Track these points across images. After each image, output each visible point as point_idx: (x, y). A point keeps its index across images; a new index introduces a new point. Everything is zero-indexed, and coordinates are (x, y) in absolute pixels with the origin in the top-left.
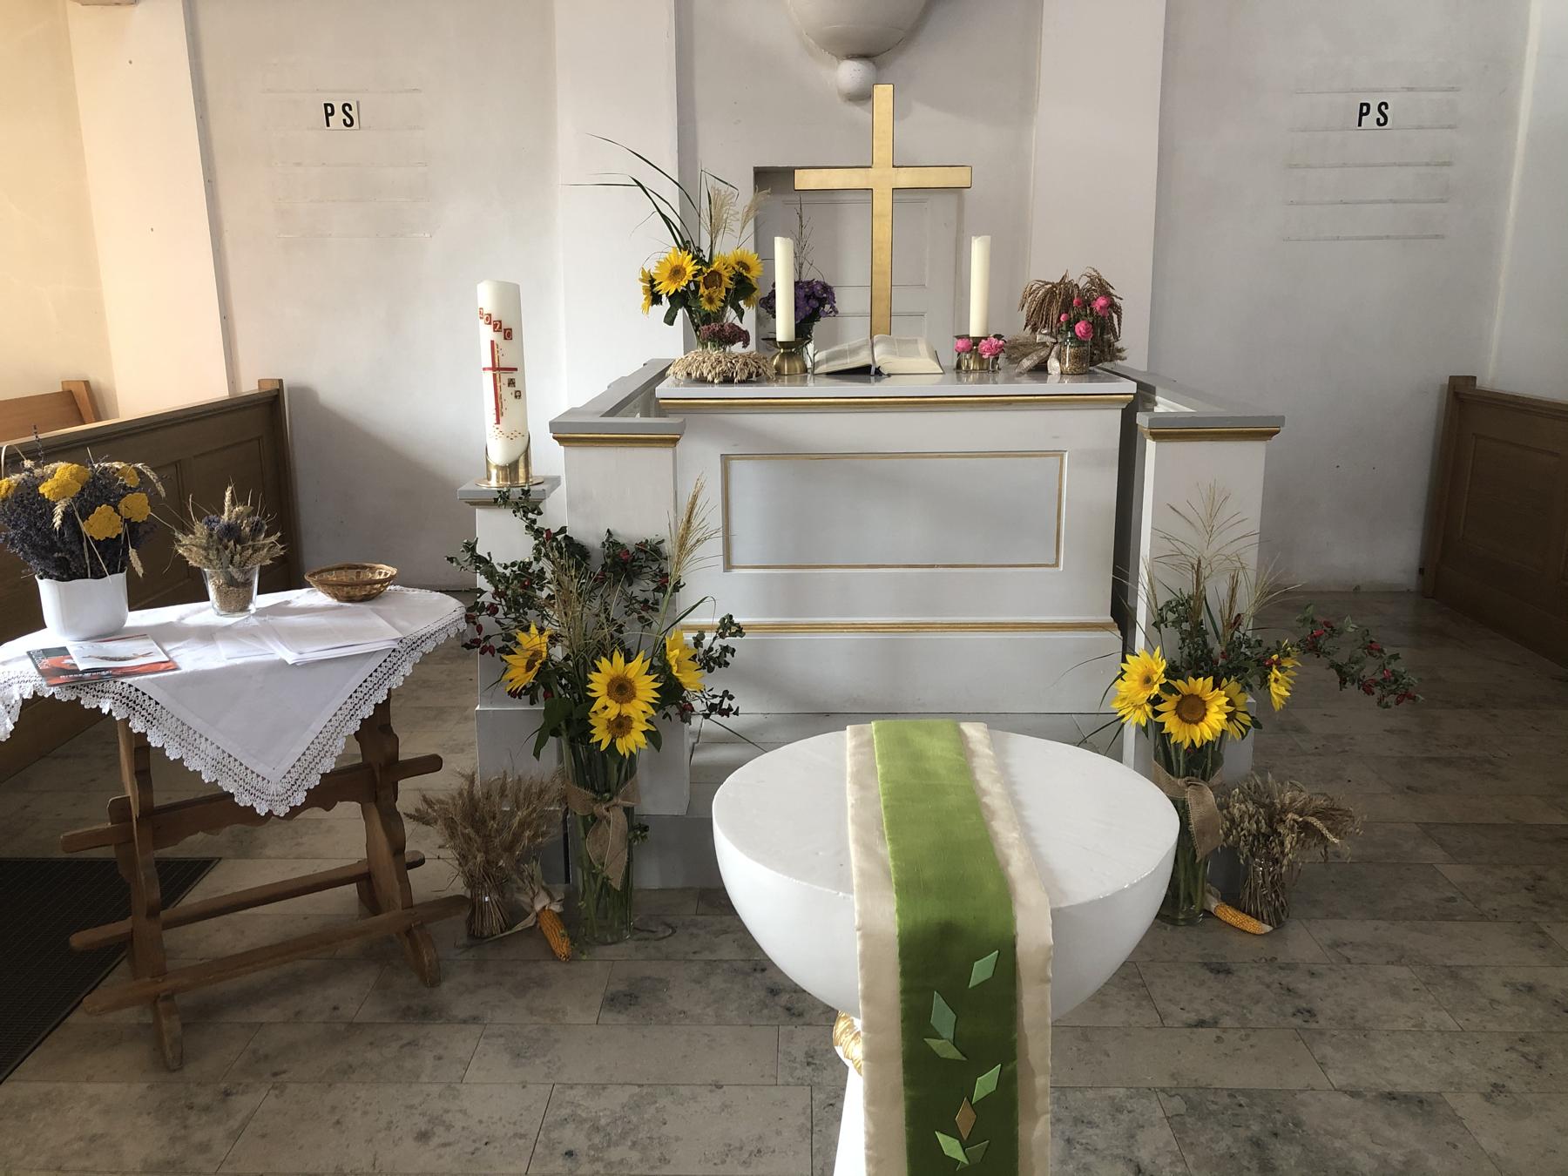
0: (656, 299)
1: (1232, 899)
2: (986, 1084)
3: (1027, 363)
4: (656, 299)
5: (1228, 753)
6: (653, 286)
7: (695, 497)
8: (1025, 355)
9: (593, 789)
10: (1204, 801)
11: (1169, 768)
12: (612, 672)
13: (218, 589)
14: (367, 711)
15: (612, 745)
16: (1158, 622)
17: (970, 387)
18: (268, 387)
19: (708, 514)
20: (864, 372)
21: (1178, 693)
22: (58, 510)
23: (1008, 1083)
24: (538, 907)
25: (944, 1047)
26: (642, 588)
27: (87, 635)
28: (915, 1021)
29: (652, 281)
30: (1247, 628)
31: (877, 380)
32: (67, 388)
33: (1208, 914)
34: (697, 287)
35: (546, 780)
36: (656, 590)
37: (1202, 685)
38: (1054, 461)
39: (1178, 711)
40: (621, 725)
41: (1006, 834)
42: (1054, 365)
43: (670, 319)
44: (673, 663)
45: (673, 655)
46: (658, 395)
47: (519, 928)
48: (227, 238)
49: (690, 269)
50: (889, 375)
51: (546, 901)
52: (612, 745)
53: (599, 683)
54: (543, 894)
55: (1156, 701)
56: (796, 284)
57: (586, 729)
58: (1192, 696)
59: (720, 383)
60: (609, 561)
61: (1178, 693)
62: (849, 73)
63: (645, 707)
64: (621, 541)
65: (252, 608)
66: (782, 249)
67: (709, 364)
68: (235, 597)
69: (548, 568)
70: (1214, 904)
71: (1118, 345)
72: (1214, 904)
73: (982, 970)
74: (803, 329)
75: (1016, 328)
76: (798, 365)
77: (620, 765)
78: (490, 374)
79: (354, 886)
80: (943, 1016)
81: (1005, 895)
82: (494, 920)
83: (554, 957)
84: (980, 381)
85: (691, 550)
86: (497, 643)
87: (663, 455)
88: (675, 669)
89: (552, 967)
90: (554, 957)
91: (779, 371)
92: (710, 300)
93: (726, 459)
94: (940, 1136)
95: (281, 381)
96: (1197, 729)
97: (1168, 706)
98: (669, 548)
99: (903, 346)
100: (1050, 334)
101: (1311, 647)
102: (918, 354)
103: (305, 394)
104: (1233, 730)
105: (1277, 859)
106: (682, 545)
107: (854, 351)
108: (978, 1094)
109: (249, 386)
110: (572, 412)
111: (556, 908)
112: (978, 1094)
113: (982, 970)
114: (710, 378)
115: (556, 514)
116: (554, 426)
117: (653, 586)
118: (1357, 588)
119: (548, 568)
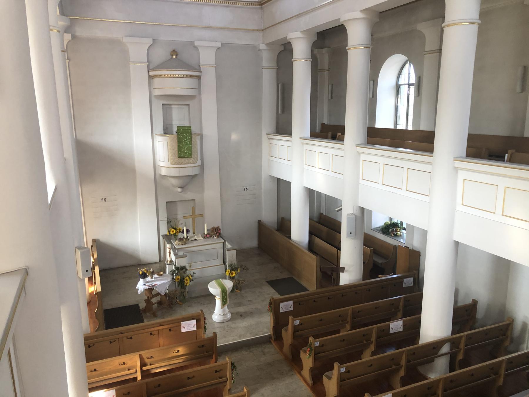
1: (237, 289)
5: (235, 277)
10: (234, 281)
11: (231, 279)
16: (229, 266)
25: (224, 295)
26: (184, 270)
30: (236, 266)
37: (233, 272)
39: (231, 274)
40: (187, 283)
41: (225, 285)
42: (215, 237)
55: (230, 273)
70: (236, 290)
72: (236, 290)
73: (225, 291)
80: (224, 294)
81: (226, 288)
83: (181, 305)
90: (181, 305)
97: (230, 274)
101: (241, 267)
104: (236, 275)
105: (142, 273)
113: (225, 291)
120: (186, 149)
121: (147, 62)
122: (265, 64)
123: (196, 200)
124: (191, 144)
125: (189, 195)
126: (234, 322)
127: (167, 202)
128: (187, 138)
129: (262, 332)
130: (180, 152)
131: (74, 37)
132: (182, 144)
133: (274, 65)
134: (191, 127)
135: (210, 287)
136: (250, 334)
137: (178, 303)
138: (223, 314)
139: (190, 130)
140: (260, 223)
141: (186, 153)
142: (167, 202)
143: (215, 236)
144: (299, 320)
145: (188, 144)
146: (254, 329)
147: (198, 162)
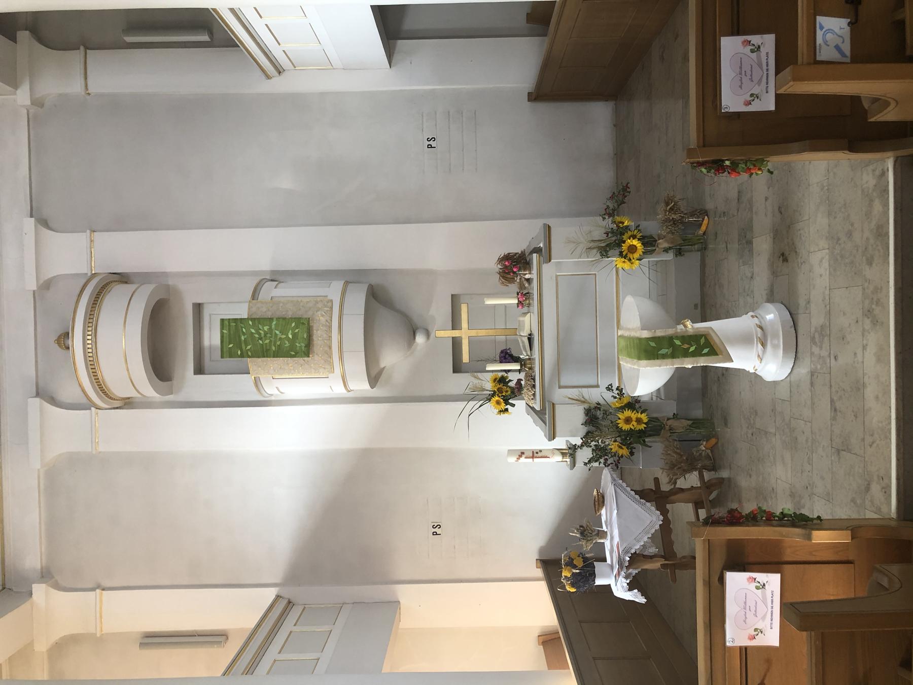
0: (506, 410)
2: (678, 342)
3: (527, 285)
4: (506, 410)
6: (503, 411)
7: (569, 398)
8: (524, 285)
9: (660, 430)
12: (622, 423)
13: (600, 539)
14: (637, 497)
15: (645, 423)
17: (535, 302)
18: (539, 565)
19: (574, 393)
20: (530, 339)
21: (627, 254)
22: (574, 571)
23: (677, 338)
24: (704, 448)
25: (669, 351)
26: (599, 414)
27: (611, 572)
28: (664, 357)
29: (501, 411)
31: (533, 335)
32: (541, 644)
33: (704, 233)
34: (503, 396)
35: (664, 446)
36: (600, 410)
37: (625, 247)
38: (559, 278)
40: (639, 421)
42: (527, 276)
43: (513, 405)
44: (620, 405)
45: (618, 405)
46: (539, 409)
47: (711, 455)
48: (482, 577)
49: (497, 398)
50: (531, 331)
51: (702, 446)
52: (645, 423)
53: (626, 427)
54: (700, 447)
56: (501, 362)
57: (640, 431)
58: (628, 249)
59: (535, 389)
60: (591, 425)
61: (627, 254)
62: (420, 339)
63: (633, 414)
64: (585, 420)
65: (606, 530)
66: (490, 367)
67: (529, 393)
68: (603, 534)
69: (593, 443)
70: (701, 232)
71: (520, 252)
73: (653, 344)
74: (516, 360)
75: (514, 288)
76: (528, 362)
77: (652, 421)
78: (535, 459)
79: (699, 510)
80: (663, 351)
82: (707, 463)
83: (717, 443)
84: (533, 299)
85: (586, 400)
86: (616, 458)
87: (557, 406)
88: (622, 405)
89: (720, 444)
90: (717, 443)
91: (530, 368)
92: (507, 391)
93: (560, 387)
94: (690, 351)
95: (537, 560)
96: (639, 247)
98: (586, 406)
99: (521, 325)
100: (517, 277)
102: (523, 321)
103: (542, 551)
106: (584, 402)
107: (523, 342)
108: (680, 344)
109: (539, 573)
110: (545, 436)
111: (705, 443)
112: (680, 344)
113: (653, 344)
114: (533, 392)
115: (578, 441)
116: (550, 440)
117: (598, 411)
118: (614, 125)
119: (593, 443)
120: (284, 336)
121: (90, 409)
122: (75, 87)
123: (453, 293)
124: (271, 319)
125: (440, 311)
126: (802, 302)
127: (454, 371)
128: (253, 331)
129: (871, 201)
130: (293, 353)
131: (46, 575)
132: (270, 346)
133: (76, 56)
134: (222, 320)
135: (634, 393)
136: (870, 262)
137: (712, 449)
138: (760, 345)
139: (229, 323)
140: (537, 96)
141: (294, 335)
142: (454, 371)
143: (525, 274)
144: (819, 19)
145: (270, 329)
146: (849, 234)
147: (330, 298)
